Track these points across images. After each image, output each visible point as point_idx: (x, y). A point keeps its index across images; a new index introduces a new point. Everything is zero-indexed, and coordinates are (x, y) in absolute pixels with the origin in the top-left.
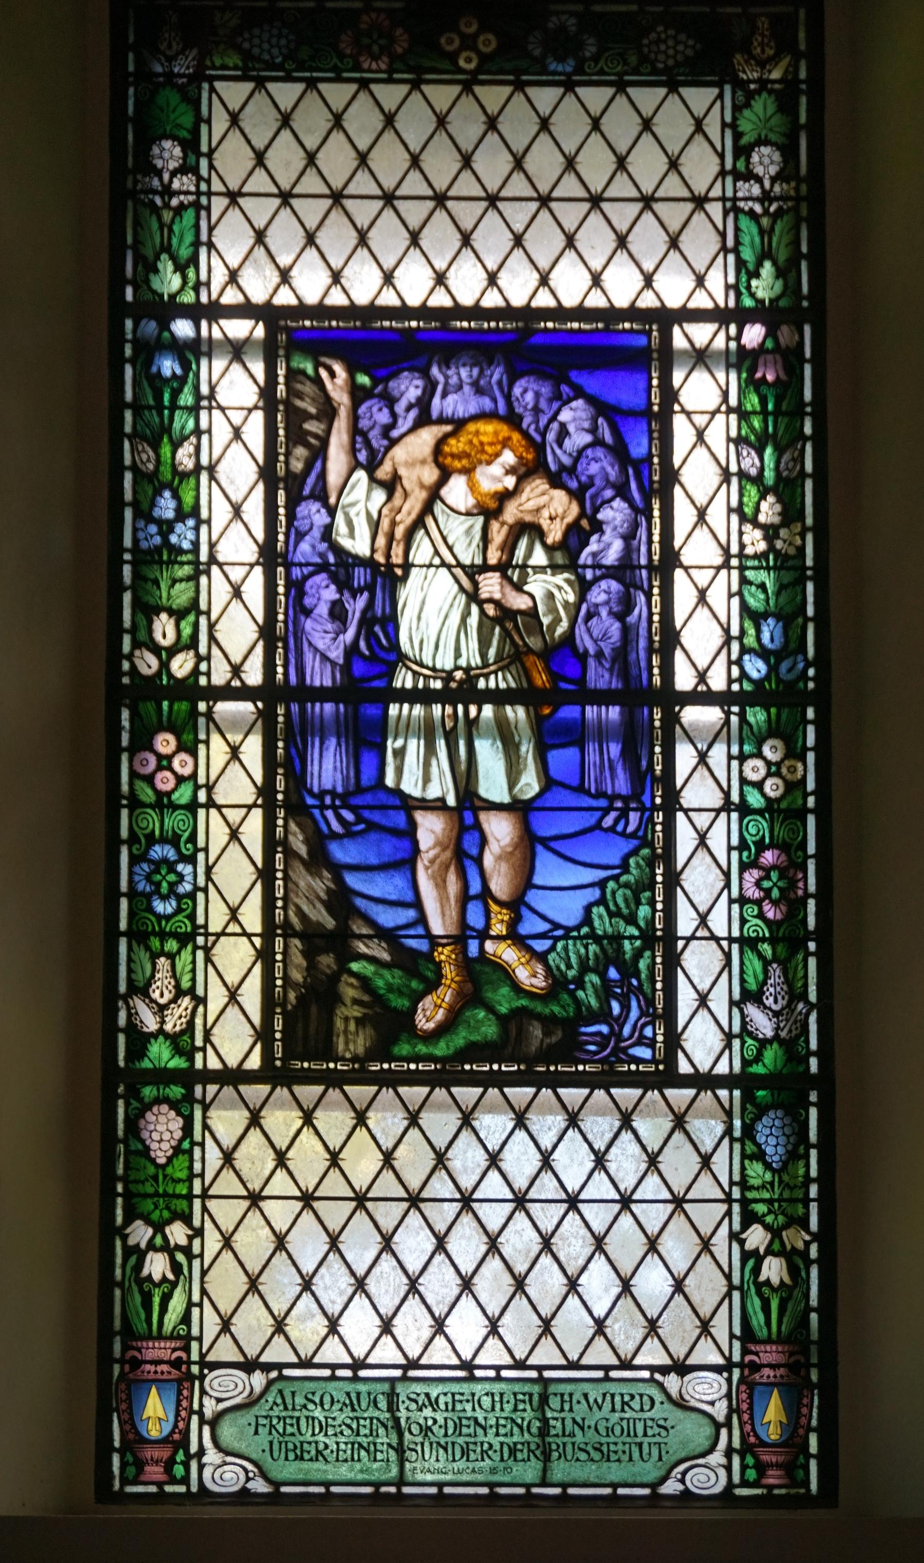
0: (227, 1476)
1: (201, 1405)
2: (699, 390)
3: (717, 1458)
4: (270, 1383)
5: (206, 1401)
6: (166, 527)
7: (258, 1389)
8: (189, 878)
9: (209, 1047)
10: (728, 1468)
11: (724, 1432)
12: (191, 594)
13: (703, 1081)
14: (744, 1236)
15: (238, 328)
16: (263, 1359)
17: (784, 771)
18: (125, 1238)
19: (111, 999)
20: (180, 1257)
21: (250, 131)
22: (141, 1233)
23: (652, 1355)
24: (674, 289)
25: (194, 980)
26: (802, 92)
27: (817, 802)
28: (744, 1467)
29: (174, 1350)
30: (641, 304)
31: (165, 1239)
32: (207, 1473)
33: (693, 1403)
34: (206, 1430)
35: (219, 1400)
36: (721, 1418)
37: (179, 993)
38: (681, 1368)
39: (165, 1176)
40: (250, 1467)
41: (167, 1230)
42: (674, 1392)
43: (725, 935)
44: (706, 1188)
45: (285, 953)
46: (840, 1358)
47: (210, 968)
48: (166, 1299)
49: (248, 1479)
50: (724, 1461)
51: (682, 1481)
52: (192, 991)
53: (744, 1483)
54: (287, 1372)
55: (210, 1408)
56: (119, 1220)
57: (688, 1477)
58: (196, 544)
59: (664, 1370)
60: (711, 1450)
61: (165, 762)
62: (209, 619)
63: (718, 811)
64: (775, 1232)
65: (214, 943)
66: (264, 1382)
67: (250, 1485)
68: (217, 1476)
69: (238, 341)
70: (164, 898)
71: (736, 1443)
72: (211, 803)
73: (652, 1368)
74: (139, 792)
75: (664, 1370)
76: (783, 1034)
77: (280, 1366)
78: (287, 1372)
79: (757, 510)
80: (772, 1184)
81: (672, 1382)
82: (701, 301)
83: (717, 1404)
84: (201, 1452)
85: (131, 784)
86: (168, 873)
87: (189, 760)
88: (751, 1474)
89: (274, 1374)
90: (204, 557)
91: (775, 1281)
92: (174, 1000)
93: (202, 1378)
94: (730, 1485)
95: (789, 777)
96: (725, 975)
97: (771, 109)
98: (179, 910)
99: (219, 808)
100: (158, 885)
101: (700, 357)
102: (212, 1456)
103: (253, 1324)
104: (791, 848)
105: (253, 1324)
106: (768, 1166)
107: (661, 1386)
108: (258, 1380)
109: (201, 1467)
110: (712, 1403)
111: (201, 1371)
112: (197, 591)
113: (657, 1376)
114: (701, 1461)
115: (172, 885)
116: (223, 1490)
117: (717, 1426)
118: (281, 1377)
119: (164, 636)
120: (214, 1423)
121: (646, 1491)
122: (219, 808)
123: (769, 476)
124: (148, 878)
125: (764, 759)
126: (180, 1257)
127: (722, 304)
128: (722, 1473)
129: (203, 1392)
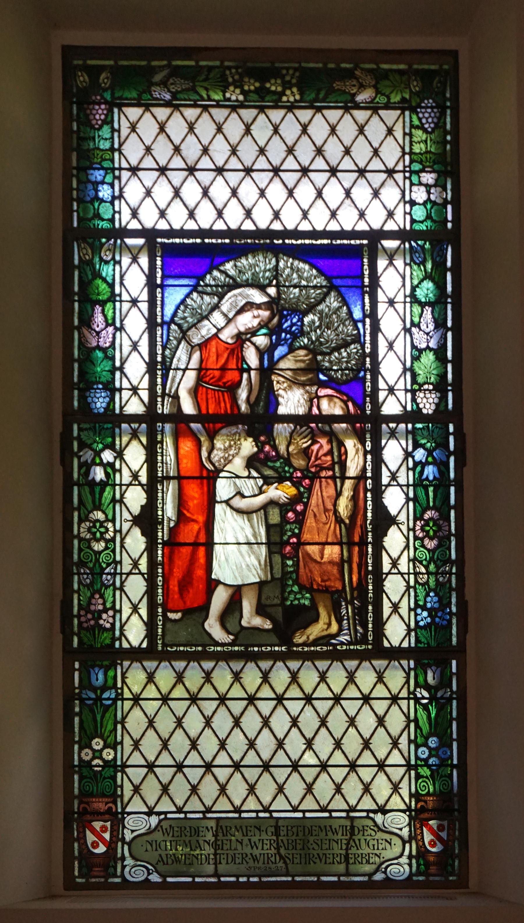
1: (123, 834)
4: (160, 821)
5: (125, 831)
7: (153, 826)
8: (112, 529)
9: (123, 638)
10: (410, 865)
11: (407, 846)
13: (395, 654)
17: (440, 753)
19: (68, 329)
20: (109, 470)
21: (141, 133)
23: (367, 804)
24: (376, 219)
25: (114, 602)
27: (453, 226)
29: (107, 803)
31: (101, 459)
32: (127, 869)
34: (126, 847)
35: (133, 831)
36: (406, 837)
37: (107, 325)
38: (383, 810)
39: (99, 136)
40: (150, 867)
41: (102, 456)
43: (407, 571)
48: (102, 491)
49: (149, 874)
50: (407, 861)
51: (385, 872)
52: (113, 608)
55: (128, 836)
56: (76, 449)
57: (389, 869)
58: (113, 625)
59: (375, 812)
64: (430, 453)
65: (126, 578)
70: (98, 541)
71: (414, 853)
73: (368, 811)
77: (166, 813)
78: (169, 816)
79: (425, 602)
81: (379, 818)
82: (391, 226)
84: (123, 858)
86: (100, 527)
87: (112, 752)
89: (162, 817)
90: (117, 633)
94: (411, 874)
95: (443, 756)
96: (406, 732)
98: (106, 548)
100: (94, 534)
102: (129, 861)
104: (443, 507)
107: (373, 820)
108: (154, 820)
109: (124, 867)
110: (401, 829)
113: (371, 815)
114: (395, 861)
115: (102, 534)
116: (134, 880)
118: (166, 818)
119: (97, 680)
124: (89, 530)
126: (109, 470)
127: (402, 227)
128: (407, 868)
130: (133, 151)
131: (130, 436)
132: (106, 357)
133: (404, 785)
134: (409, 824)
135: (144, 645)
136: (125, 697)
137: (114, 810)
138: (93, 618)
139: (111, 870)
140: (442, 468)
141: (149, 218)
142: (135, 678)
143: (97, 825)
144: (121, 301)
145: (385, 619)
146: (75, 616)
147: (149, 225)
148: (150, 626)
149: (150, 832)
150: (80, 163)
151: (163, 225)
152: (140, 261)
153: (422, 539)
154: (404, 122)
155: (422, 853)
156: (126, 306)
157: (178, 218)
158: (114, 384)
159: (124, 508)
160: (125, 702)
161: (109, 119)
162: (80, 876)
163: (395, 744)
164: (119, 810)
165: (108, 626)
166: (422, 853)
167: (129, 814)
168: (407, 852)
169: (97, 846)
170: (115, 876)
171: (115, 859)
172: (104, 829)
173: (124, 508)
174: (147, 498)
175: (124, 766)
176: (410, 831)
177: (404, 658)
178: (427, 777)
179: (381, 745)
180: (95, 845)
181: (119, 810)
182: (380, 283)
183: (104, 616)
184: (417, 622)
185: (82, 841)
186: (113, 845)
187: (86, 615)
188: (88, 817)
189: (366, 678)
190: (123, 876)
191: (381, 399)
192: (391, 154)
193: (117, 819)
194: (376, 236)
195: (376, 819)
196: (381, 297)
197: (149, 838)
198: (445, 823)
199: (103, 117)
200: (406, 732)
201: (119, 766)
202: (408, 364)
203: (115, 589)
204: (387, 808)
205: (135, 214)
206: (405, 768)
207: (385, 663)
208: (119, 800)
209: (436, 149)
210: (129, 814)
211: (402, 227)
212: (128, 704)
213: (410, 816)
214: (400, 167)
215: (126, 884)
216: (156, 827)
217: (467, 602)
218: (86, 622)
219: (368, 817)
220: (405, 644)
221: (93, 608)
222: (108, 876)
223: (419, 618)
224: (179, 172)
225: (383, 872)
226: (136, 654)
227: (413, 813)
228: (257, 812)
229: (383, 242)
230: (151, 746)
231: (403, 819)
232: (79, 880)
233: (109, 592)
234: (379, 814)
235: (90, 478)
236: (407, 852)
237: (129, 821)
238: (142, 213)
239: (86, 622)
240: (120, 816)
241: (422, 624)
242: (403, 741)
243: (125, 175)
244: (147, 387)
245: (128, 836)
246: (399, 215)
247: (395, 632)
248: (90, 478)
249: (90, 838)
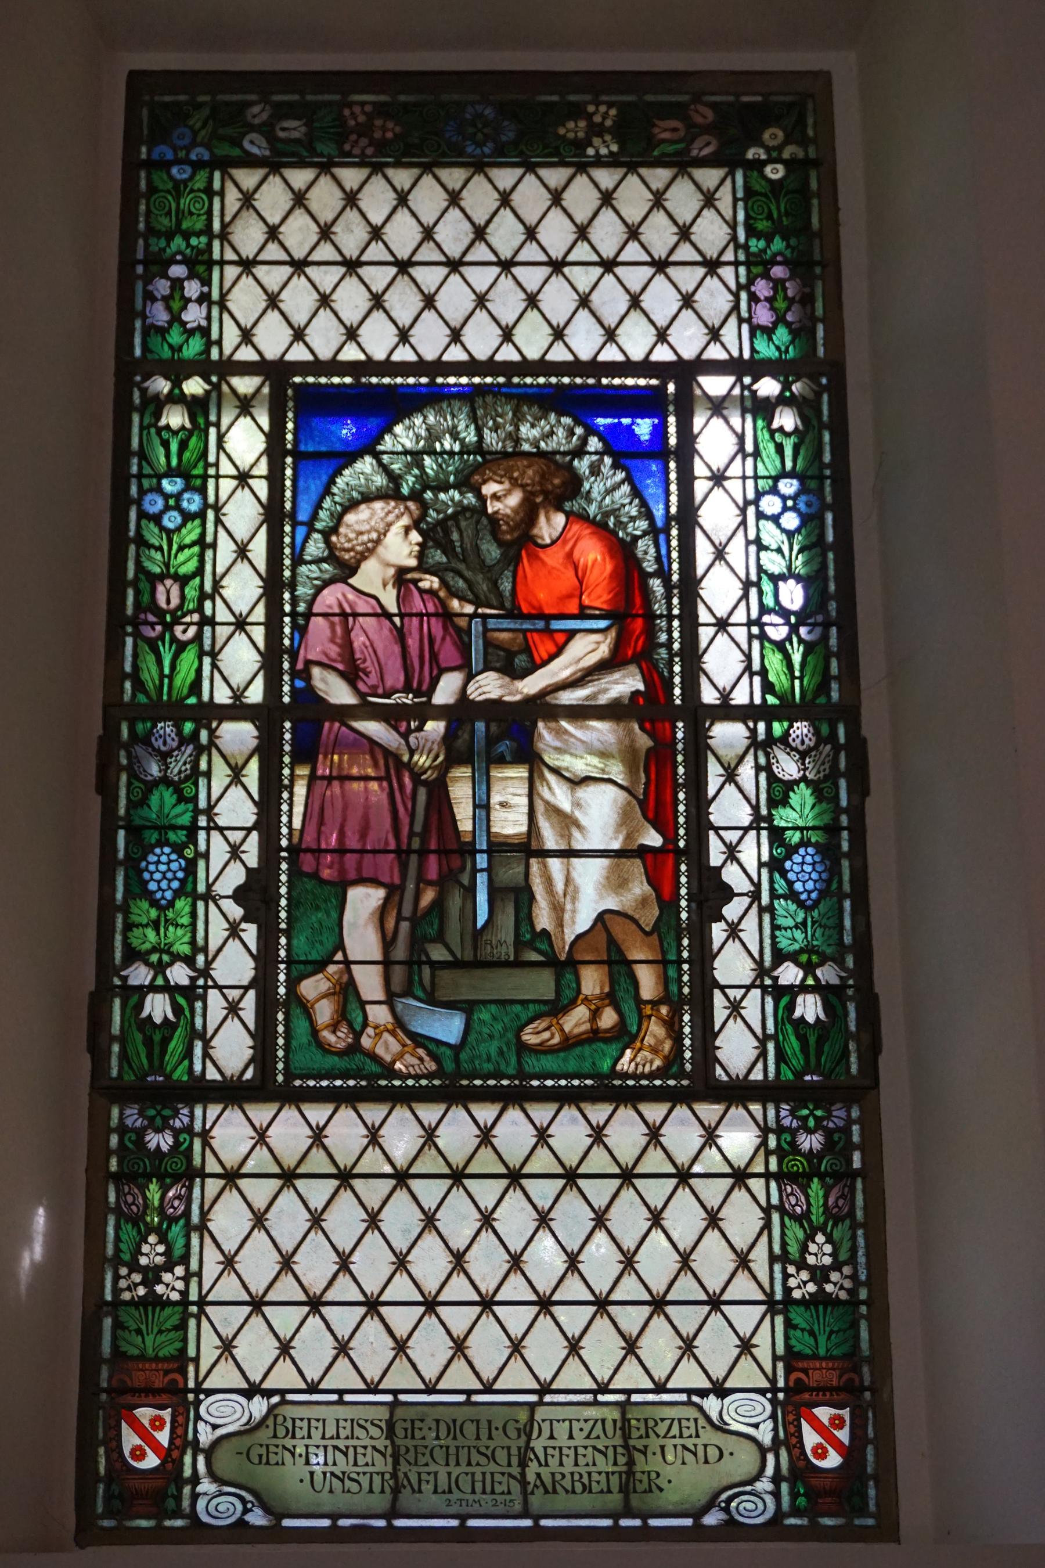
0: (221, 1508)
1: (196, 1431)
2: (715, 440)
3: (764, 1485)
4: (271, 1409)
5: (201, 1426)
6: (152, 1276)
7: (257, 1415)
10: (776, 1494)
12: (198, 531)
14: (775, 973)
15: (245, 385)
16: (264, 1386)
18: (144, 317)
22: (140, 975)
23: (689, 1376)
24: (688, 340)
26: (863, 1316)
28: (794, 1495)
29: (167, 1372)
30: (655, 357)
32: (201, 1504)
33: (735, 1427)
35: (215, 1427)
38: (721, 1391)
39: (166, 921)
42: (714, 1416)
44: (743, 1287)
45: (288, 1035)
46: (835, 100)
47: (216, 675)
48: (166, 1041)
49: (246, 1511)
50: (770, 1487)
51: (727, 1510)
53: (795, 1512)
54: (290, 1397)
55: (206, 1436)
57: (733, 1504)
59: (703, 1393)
60: (758, 1477)
61: (173, 502)
62: (206, 956)
63: (746, 830)
66: (265, 1410)
67: (248, 1517)
68: (211, 1508)
69: (246, 396)
72: (213, 826)
73: (690, 1392)
74: (145, 533)
75: (703, 1393)
76: (810, 776)
77: (282, 1392)
80: (804, 923)
81: (712, 1405)
83: (761, 1426)
84: (195, 1480)
85: (138, 526)
87: (197, 498)
88: (802, 1501)
89: (276, 1399)
91: (810, 1019)
92: (178, 748)
93: (198, 1403)
96: (764, 1238)
97: (810, 801)
99: (221, 830)
101: (718, 407)
102: (206, 1486)
103: (255, 1350)
105: (255, 1350)
106: (801, 904)
107: (700, 1408)
108: (259, 1406)
109: (195, 1497)
110: (756, 1426)
111: (197, 1397)
112: (185, 1340)
113: (695, 1399)
114: (748, 1488)
117: (763, 1451)
120: (210, 1453)
121: (688, 1522)
122: (221, 830)
123: (817, 1216)
125: (782, 513)
127: (735, 354)
128: (769, 1499)
129: (198, 1417)
130: (248, 237)
131: (237, 411)
132: (181, 799)
133: (763, 1339)
134: (773, 1416)
135: (249, 1075)
136: (208, 1170)
137: (181, 1385)
138: (143, 1283)
139: (171, 1503)
140: (808, 412)
141: (273, 340)
142: (230, 1133)
143: (145, 1414)
144: (217, 477)
145: (717, 1029)
146: (134, 476)
147: (272, 353)
148: (262, 1037)
149: (252, 1428)
150: (155, 247)
151: (299, 354)
152: (255, 412)
153: (793, 1132)
154: (734, 182)
155: (801, 1471)
156: (227, 486)
157: (324, 340)
158: (211, 253)
159: (207, 1240)
160: (221, 480)
161: (189, 887)
162: (109, 1513)
163: (743, 1261)
164: (191, 1384)
165: (175, 1296)
166: (801, 1471)
167: (210, 1392)
168: (770, 1470)
169: (142, 1456)
170: (177, 1514)
171: (179, 1481)
172: (158, 1423)
173: (207, 1240)
174: (255, 969)
175: (202, 1302)
176: (775, 1429)
177: (755, 1100)
178: (765, 195)
179: (714, 1262)
180: (139, 1454)
181: (191, 1384)
182: (700, 520)
183: (167, 1277)
184: (787, 1290)
185: (114, 1444)
186: (175, 1454)
187: (129, 1275)
188: (129, 1399)
189: (682, 1134)
190: (193, 1515)
191: (698, 496)
192: (712, 233)
193: (181, 1397)
194: (687, 371)
195: (706, 1407)
196: (699, 469)
197: (247, 1441)
198: (845, 1413)
199: (175, 885)
200: (764, 1238)
201: (193, 1303)
202: (764, 812)
203: (189, 1228)
204: (728, 1385)
205: (247, 336)
206: (763, 1308)
207: (718, 1108)
208: (191, 1369)
209: (805, 564)
210: (210, 1392)
211: (735, 354)
212: (213, 1186)
213: (774, 1402)
214: (740, 616)
215: (199, 1531)
216: (265, 1418)
217: (864, 741)
218: (129, 1289)
219: (689, 1403)
220: (757, 1075)
221: (143, 1261)
222: (162, 1514)
223: (792, 1282)
224: (327, 271)
225: (722, 1509)
226: (233, 1093)
227: (781, 1396)
228: (469, 1393)
229: (701, 379)
230: (258, 1265)
231: (762, 1406)
232: (106, 1523)
233: (176, 1229)
234: (712, 1397)
235: (144, 1014)
236: (770, 1470)
237: (212, 1408)
238: (261, 337)
239: (129, 1289)
240: (191, 1397)
241: (797, 1294)
242: (759, 1257)
243: (231, 272)
244: (262, 619)
245: (206, 1436)
246: (729, 334)
247: (736, 1050)
248: (144, 1014)
249: (130, 1440)
